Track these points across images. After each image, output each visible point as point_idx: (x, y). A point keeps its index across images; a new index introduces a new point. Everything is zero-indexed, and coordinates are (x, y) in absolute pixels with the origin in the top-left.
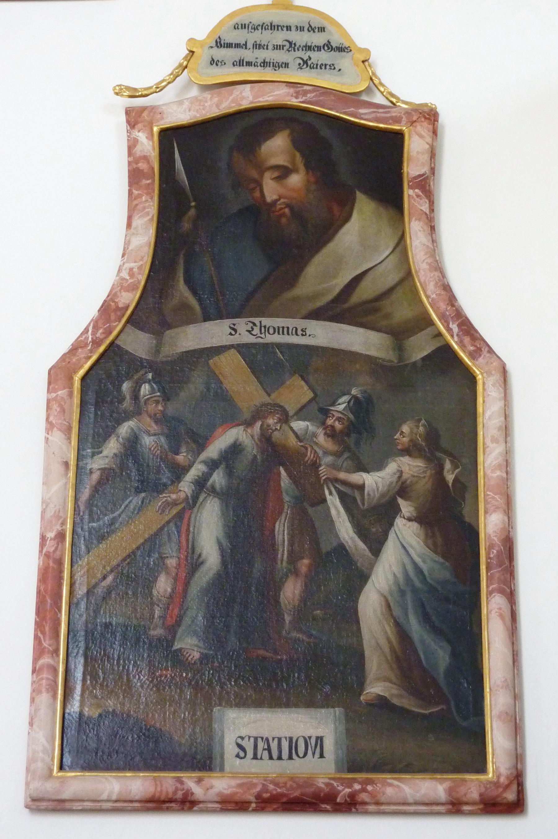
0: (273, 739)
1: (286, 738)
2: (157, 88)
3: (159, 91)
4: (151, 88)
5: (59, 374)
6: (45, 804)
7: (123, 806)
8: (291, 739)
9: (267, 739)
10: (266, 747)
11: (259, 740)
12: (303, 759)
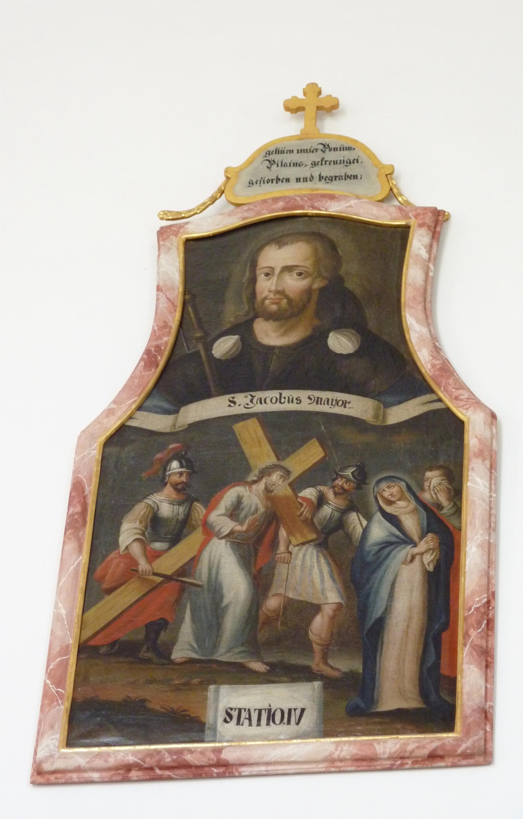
0: (255, 710)
1: (245, 710)
2: (198, 209)
3: (200, 212)
4: (193, 210)
5: (87, 435)
6: (44, 775)
7: (123, 773)
8: (270, 710)
9: (249, 710)
10: (247, 717)
11: (243, 710)
12: (279, 726)
